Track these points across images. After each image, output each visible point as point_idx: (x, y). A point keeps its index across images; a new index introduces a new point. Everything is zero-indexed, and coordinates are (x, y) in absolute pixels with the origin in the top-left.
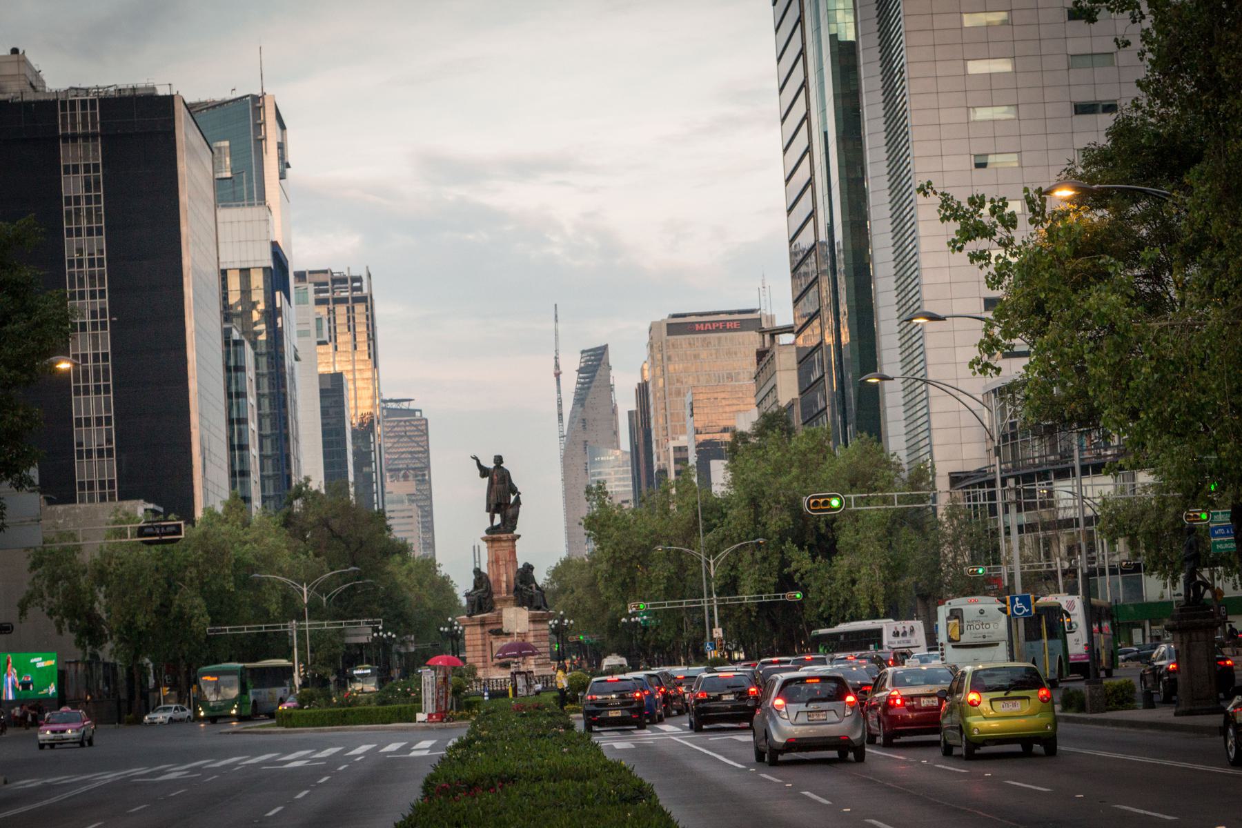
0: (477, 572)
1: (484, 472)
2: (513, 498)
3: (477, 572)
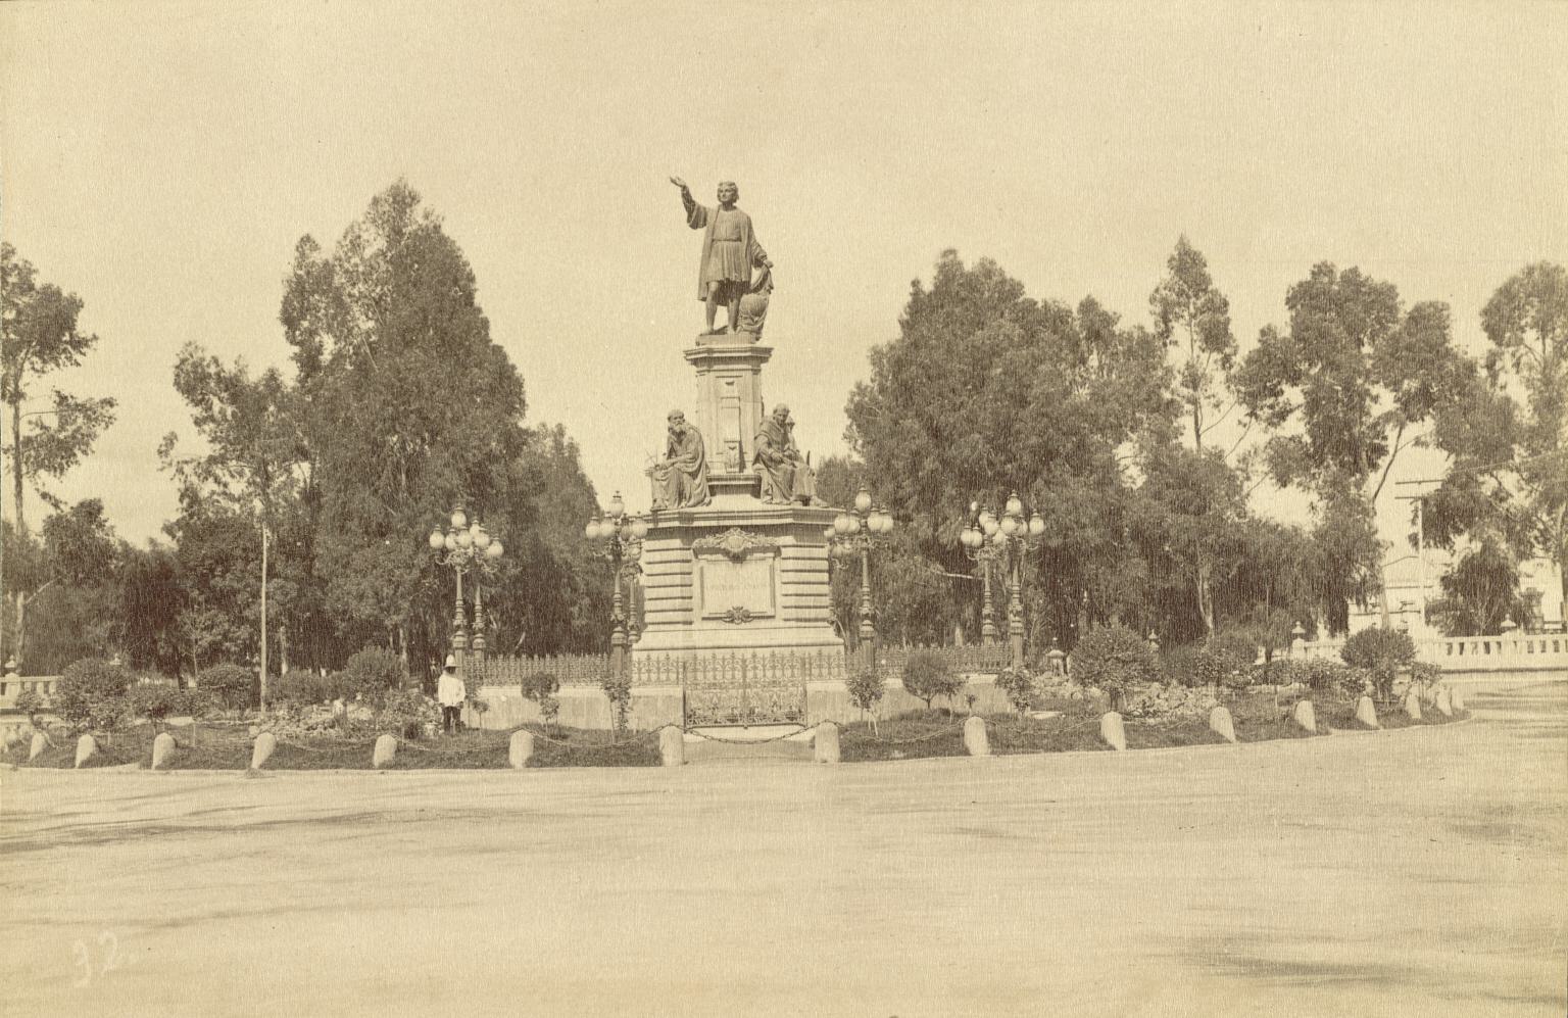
1: (696, 217)
2: (756, 274)
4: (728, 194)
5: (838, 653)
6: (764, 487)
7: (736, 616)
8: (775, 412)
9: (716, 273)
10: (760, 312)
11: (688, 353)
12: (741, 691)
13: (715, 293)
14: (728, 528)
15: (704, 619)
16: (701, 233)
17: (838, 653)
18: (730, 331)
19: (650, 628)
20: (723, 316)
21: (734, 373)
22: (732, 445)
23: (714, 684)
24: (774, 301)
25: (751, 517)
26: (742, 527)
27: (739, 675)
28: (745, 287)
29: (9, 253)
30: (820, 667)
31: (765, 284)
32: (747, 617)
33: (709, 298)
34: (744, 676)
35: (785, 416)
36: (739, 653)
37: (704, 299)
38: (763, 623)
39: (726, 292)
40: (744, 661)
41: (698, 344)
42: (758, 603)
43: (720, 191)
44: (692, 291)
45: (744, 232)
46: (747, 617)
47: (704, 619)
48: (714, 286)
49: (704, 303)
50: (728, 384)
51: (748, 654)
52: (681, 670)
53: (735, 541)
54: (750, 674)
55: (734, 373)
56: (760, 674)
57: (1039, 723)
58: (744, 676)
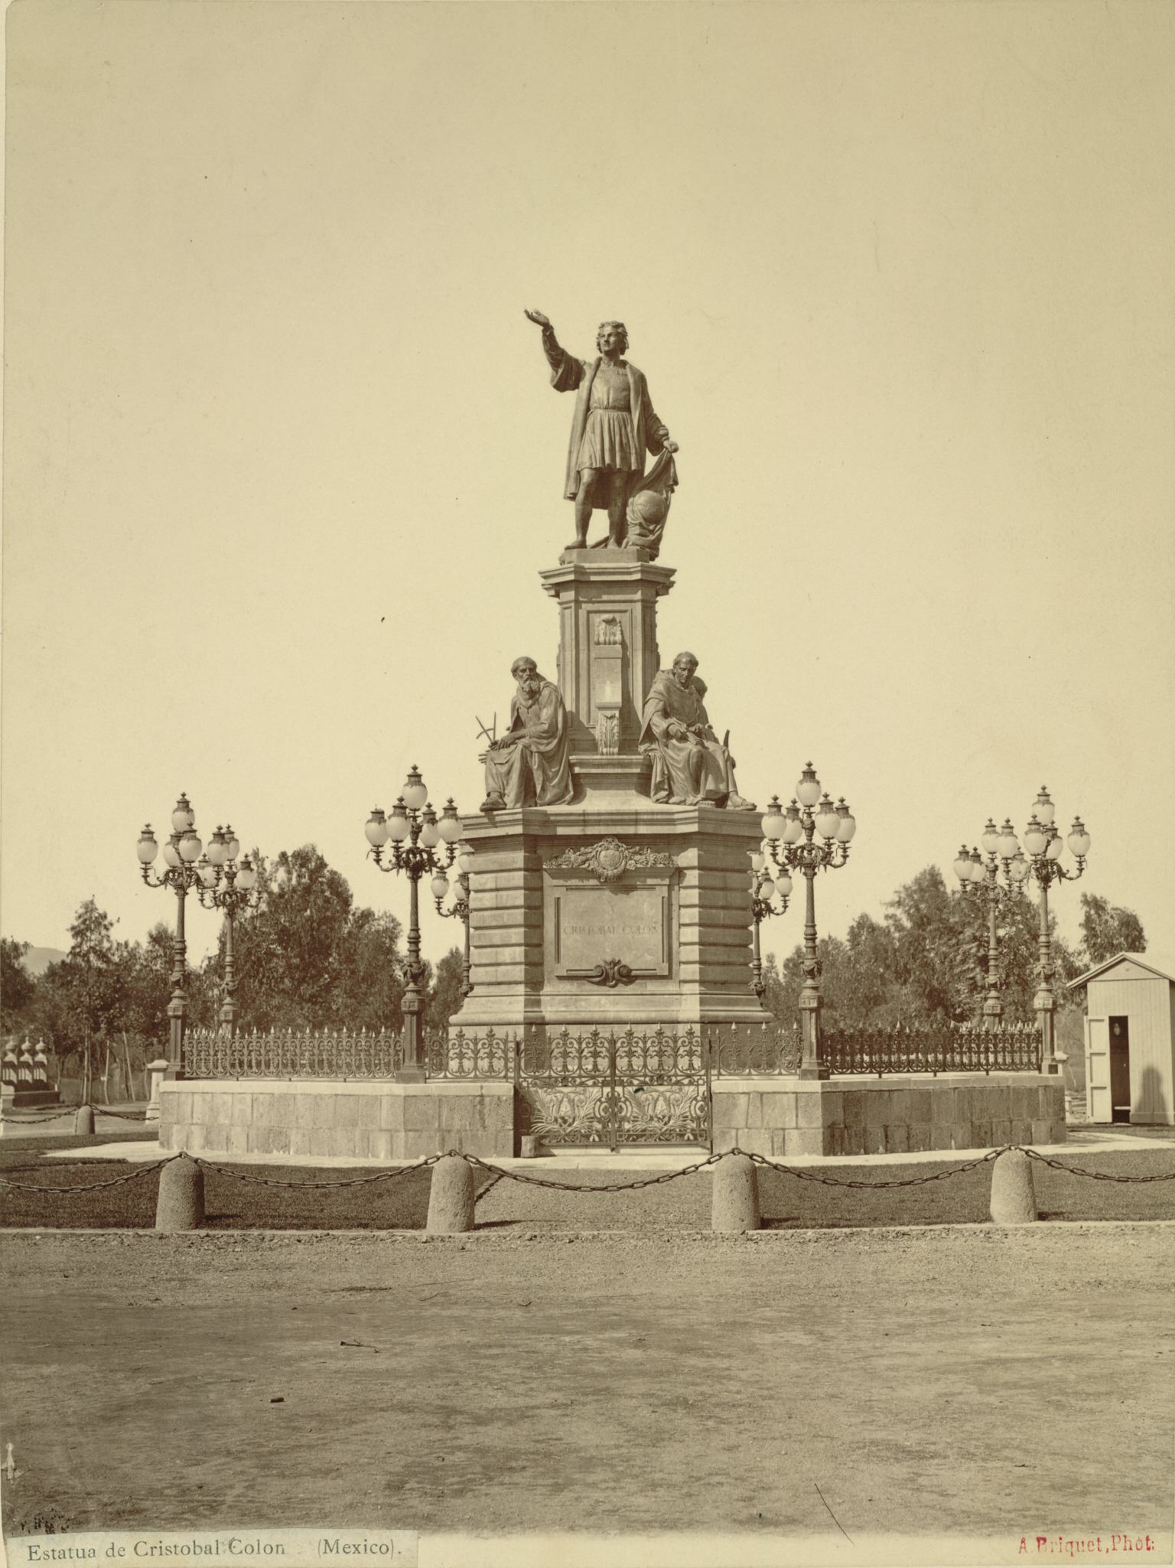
0: (527, 670)
1: (567, 373)
2: (651, 461)
3: (527, 670)
4: (612, 339)
5: (691, 1033)
6: (656, 777)
7: (611, 973)
8: (677, 663)
9: (590, 455)
10: (657, 518)
11: (546, 576)
12: (607, 1090)
13: (589, 485)
14: (599, 838)
15: (560, 978)
16: (571, 399)
17: (691, 1033)
18: (612, 545)
19: (477, 990)
20: (600, 523)
21: (616, 607)
22: (609, 713)
23: (660, 1077)
24: (679, 501)
25: (636, 822)
26: (621, 838)
27: (603, 1063)
28: (634, 480)
29: (4, 941)
30: (461, 1056)
31: (665, 478)
32: (627, 976)
33: (580, 496)
34: (613, 1065)
35: (691, 671)
36: (605, 1032)
37: (573, 497)
38: (652, 987)
39: (603, 488)
40: (613, 1042)
41: (563, 562)
42: (644, 954)
43: (601, 335)
44: (557, 482)
45: (635, 395)
46: (627, 976)
47: (560, 978)
48: (586, 476)
49: (572, 504)
50: (608, 622)
51: (482, 1032)
52: (511, 1055)
53: (606, 857)
54: (622, 1063)
55: (616, 607)
56: (637, 1063)
57: (161, 1056)
58: (613, 1065)
